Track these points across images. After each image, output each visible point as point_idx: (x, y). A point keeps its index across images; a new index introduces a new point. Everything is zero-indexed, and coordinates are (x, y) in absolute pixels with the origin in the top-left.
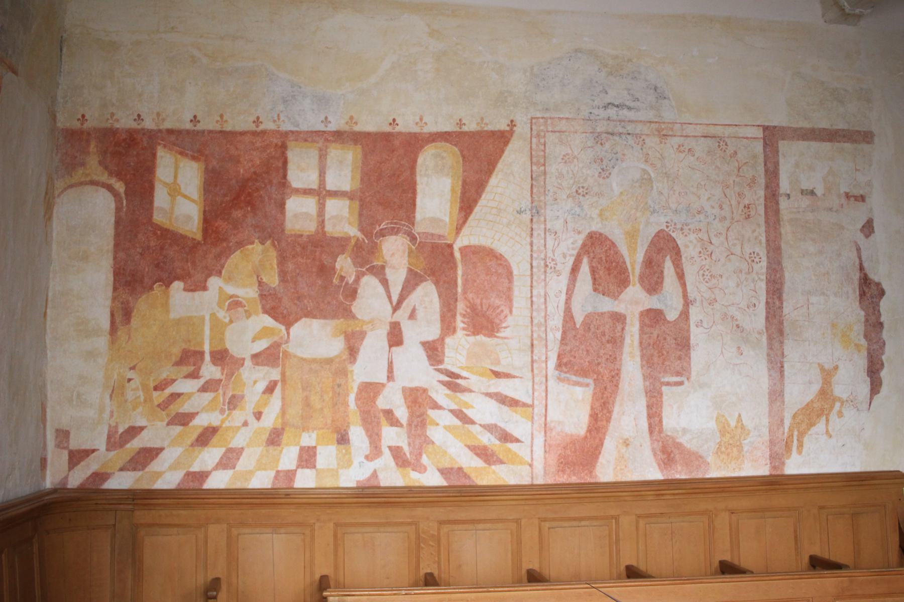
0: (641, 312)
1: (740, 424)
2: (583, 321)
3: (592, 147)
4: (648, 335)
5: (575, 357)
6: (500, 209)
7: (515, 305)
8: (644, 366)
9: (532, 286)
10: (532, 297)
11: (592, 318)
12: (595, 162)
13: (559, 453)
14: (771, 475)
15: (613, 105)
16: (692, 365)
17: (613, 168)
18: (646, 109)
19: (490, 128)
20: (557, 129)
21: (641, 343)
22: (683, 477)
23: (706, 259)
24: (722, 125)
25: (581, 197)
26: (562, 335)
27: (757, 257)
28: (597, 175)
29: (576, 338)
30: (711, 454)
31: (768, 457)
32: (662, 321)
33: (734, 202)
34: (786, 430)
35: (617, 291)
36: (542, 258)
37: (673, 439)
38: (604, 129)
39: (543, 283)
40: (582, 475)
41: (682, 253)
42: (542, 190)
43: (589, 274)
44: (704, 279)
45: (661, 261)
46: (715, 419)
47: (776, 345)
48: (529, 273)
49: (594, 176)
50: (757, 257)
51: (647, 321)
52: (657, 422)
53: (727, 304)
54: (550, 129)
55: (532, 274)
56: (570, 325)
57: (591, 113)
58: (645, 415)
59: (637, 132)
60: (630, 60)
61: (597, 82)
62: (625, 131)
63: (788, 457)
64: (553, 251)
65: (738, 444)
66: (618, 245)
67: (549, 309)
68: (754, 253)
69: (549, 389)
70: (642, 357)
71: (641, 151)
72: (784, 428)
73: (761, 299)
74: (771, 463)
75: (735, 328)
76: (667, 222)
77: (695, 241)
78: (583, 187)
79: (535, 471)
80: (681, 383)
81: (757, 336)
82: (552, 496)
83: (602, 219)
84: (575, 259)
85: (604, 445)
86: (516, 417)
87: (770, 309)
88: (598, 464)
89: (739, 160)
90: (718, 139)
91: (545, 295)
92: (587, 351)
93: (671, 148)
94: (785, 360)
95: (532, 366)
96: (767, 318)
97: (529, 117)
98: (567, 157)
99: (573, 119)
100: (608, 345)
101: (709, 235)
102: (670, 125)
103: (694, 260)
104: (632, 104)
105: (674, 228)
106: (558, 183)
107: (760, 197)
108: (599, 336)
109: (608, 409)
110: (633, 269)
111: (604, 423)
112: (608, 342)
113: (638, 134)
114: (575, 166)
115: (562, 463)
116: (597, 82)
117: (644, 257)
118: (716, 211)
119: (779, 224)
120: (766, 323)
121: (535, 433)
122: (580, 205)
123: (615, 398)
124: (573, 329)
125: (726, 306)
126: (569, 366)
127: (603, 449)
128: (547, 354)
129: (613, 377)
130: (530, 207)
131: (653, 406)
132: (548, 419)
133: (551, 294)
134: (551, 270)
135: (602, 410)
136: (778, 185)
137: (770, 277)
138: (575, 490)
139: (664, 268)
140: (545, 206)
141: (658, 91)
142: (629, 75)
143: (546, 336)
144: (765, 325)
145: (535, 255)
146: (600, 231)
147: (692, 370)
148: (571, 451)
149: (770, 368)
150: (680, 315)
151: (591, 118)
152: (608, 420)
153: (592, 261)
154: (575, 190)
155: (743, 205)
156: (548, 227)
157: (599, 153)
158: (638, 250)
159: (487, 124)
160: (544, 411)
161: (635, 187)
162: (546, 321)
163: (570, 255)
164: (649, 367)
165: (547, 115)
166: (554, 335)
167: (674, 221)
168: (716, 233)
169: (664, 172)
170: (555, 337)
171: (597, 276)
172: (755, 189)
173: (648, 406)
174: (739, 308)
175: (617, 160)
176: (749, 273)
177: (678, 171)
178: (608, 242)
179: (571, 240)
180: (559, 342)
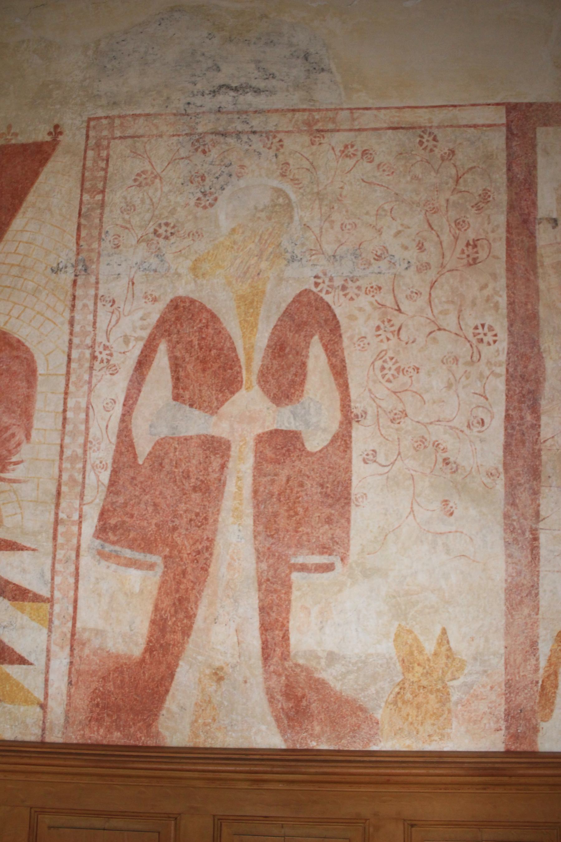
0: (259, 436)
1: (443, 649)
2: (150, 453)
3: (187, 158)
4: (269, 478)
5: (132, 516)
6: (24, 267)
7: (37, 424)
8: (259, 533)
9: (66, 393)
10: (65, 411)
11: (167, 446)
12: (192, 183)
13: (94, 686)
14: (508, 753)
15: (229, 87)
16: (352, 533)
17: (223, 189)
18: (288, 91)
19: (22, 139)
20: (130, 132)
21: (255, 492)
22: (324, 746)
23: (388, 339)
24: (427, 107)
25: (161, 241)
26: (111, 476)
27: (490, 334)
28: (192, 202)
29: (135, 482)
30: (383, 705)
31: (503, 716)
32: (298, 453)
33: (446, 238)
34: (543, 663)
35: (217, 399)
36: (87, 345)
37: (308, 671)
38: (210, 127)
39: (86, 387)
40: (132, 730)
41: (343, 329)
42: (95, 233)
43: (168, 371)
44: (383, 377)
45: (303, 344)
46: (393, 636)
47: (524, 496)
48: (64, 371)
49: (187, 204)
50: (490, 334)
51: (269, 453)
52: (278, 639)
53: (427, 420)
54: (118, 134)
55: (68, 373)
56: (125, 460)
57: (189, 103)
58: (257, 624)
59: (268, 129)
60: (264, 16)
61: (203, 54)
62: (247, 128)
63: (547, 718)
64: (108, 333)
65: (439, 686)
66: (222, 320)
67: (91, 431)
68: (483, 326)
69: (82, 571)
70: (257, 517)
71: (274, 160)
72: (537, 660)
73: (495, 410)
74: (507, 728)
75: (440, 464)
76: (316, 277)
77: (368, 308)
78: (167, 224)
79: (50, 716)
80: (328, 568)
81: (487, 480)
82: (65, 770)
83: (196, 276)
84: (145, 346)
85: (176, 677)
86: (23, 619)
87: (513, 428)
88: (164, 712)
89: (458, 163)
90: (419, 132)
91: (88, 408)
92: (155, 505)
93: (331, 151)
94: (541, 525)
95: (55, 530)
96: (507, 446)
97: (85, 118)
98: (144, 176)
99: (156, 115)
100: (193, 496)
101: (395, 297)
102: (330, 114)
103: (366, 341)
104: (262, 85)
105: (328, 286)
106: (123, 219)
107: (498, 226)
108: (178, 478)
109: (187, 612)
110: (249, 359)
111: (178, 636)
112: (195, 489)
113: (271, 131)
114: (156, 190)
115: (98, 705)
116: (203, 54)
117: (270, 339)
118: (412, 254)
119: (535, 273)
120: (505, 457)
121: (53, 648)
122: (159, 254)
123: (200, 592)
124: (131, 467)
125: (425, 425)
126: (121, 531)
127: (174, 683)
128: (81, 510)
129: (199, 553)
130: (73, 261)
131: (271, 608)
132: (78, 625)
133: (98, 405)
134: (102, 365)
135: (176, 612)
136: (534, 204)
137: (515, 369)
138: (283, 766)
139: (307, 357)
140: (98, 259)
141: (311, 59)
142: (260, 38)
143: (84, 478)
144: (502, 459)
145: (76, 341)
146: (191, 296)
147: (352, 542)
148: (114, 684)
149: (510, 541)
150: (333, 441)
151: (189, 111)
152: (187, 631)
153: (174, 347)
154: (152, 230)
155: (465, 243)
156: (101, 293)
157: (199, 167)
158: (260, 326)
159: (16, 135)
160: (71, 609)
161: (259, 218)
162: (85, 451)
163: (137, 339)
164: (268, 536)
165: (115, 112)
166: (98, 476)
167: (329, 275)
168: (409, 292)
169: (315, 190)
170: (98, 480)
171: (182, 374)
172: (488, 212)
173: (262, 609)
174: (451, 428)
175: (230, 175)
176: (472, 363)
177: (342, 188)
178: (204, 315)
179: (140, 314)
180: (105, 489)
